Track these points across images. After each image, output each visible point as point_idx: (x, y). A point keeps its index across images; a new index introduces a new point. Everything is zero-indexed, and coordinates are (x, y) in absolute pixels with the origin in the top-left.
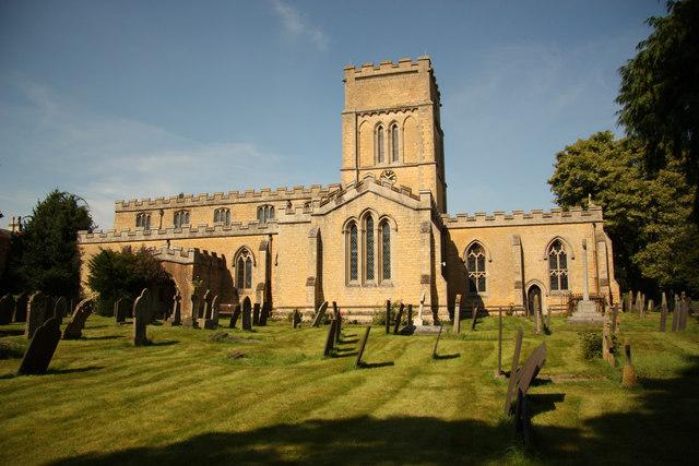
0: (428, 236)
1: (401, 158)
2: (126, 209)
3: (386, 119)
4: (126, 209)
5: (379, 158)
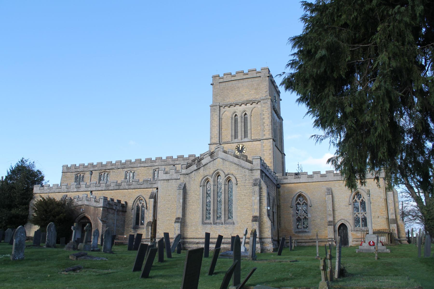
0: (257, 188)
1: (249, 135)
2: (69, 170)
3: (239, 110)
4: (69, 170)
5: (236, 137)
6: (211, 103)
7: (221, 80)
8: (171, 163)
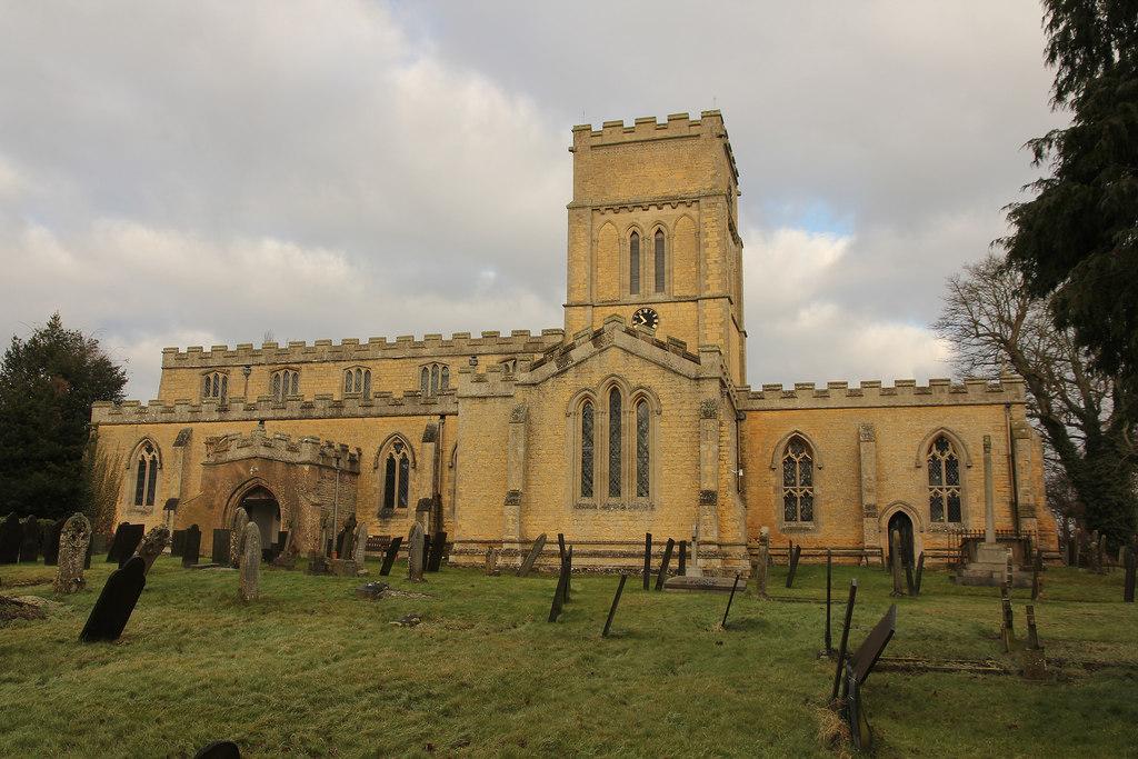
2: (183, 363)
3: (646, 219)
4: (183, 363)
5: (634, 288)
6: (569, 199)
7: (597, 141)
8: (468, 350)
